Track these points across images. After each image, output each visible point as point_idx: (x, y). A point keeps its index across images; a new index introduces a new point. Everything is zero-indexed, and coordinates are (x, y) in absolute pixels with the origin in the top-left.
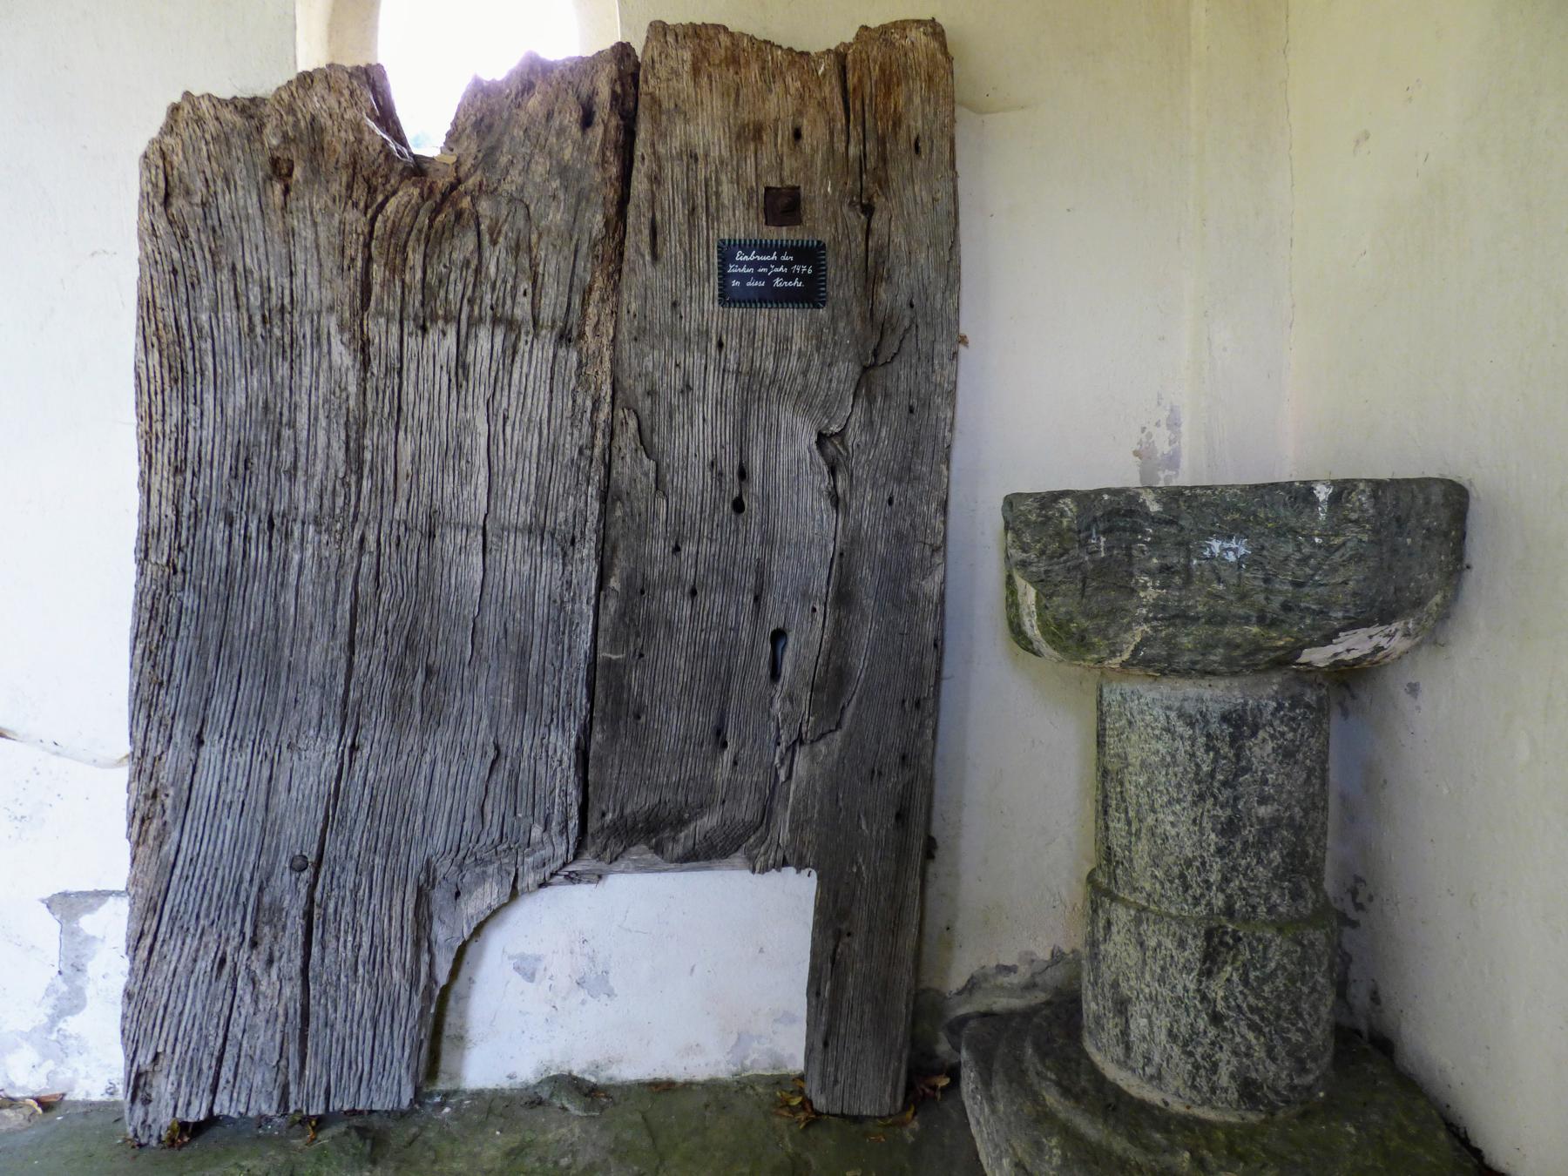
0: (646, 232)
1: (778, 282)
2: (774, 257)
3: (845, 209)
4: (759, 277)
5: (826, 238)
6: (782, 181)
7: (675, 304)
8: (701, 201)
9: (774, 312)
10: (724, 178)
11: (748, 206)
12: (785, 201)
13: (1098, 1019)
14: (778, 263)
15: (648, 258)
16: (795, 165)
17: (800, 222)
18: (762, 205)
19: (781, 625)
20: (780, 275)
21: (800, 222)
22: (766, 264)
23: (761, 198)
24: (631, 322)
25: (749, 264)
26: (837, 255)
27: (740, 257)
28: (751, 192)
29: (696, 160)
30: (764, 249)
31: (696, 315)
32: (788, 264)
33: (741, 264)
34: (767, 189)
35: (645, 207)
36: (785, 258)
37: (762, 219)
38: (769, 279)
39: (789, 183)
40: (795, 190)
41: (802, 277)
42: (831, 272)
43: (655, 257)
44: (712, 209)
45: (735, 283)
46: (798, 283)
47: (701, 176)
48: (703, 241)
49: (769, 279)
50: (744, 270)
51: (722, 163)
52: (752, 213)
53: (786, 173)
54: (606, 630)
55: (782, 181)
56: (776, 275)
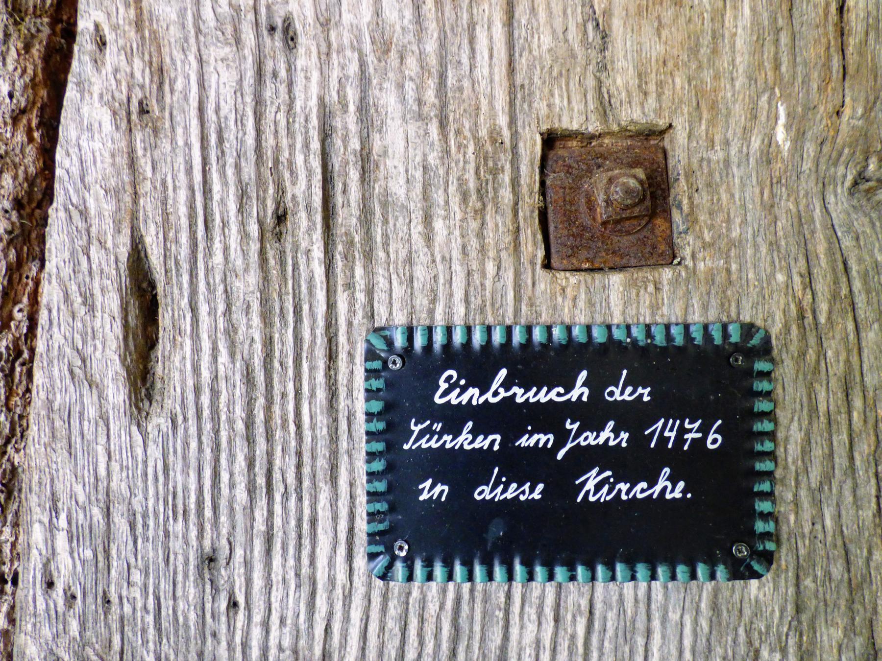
0: (110, 301)
1: (592, 484)
2: (580, 391)
3: (839, 202)
4: (517, 465)
5: (774, 318)
6: (605, 107)
7: (210, 560)
8: (304, 188)
9: (576, 594)
10: (387, 99)
11: (479, 202)
12: (622, 183)
13: (840, 413)
14: (592, 414)
15: (117, 394)
16: (655, 49)
17: (669, 256)
18: (530, 201)
19: (548, 584)
20: (600, 456)
21: (669, 256)
22: (548, 417)
23: (529, 174)
24: (58, 619)
25: (485, 418)
26: (813, 375)
27: (451, 391)
28: (491, 154)
29: (290, 39)
30: (539, 361)
31: (288, 600)
32: (631, 417)
33: (454, 418)
34: (550, 140)
35: (101, 206)
36: (619, 394)
37: (532, 247)
38: (561, 475)
39: (633, 113)
40: (652, 135)
41: (687, 462)
42: (792, 434)
43: (142, 379)
44: (347, 217)
45: (432, 491)
46: (668, 487)
47: (307, 99)
48: (313, 333)
49: (561, 475)
50: (464, 440)
51: (384, 48)
52: (497, 225)
53: (622, 79)
54: (288, 294)
55: (605, 107)
56: (585, 458)
